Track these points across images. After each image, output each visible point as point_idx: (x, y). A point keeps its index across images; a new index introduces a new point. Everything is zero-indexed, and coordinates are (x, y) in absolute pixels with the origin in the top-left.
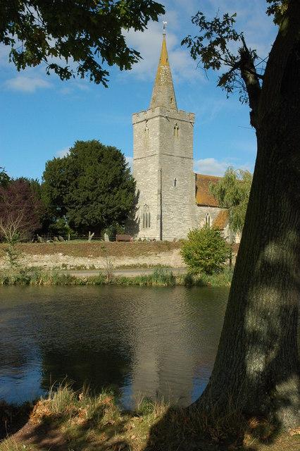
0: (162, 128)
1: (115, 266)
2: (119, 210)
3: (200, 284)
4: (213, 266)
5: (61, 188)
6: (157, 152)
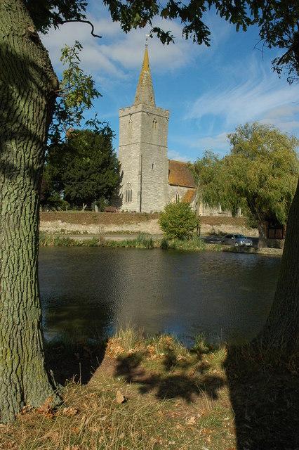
0: (143, 119)
2: (107, 186)
3: (174, 248)
4: (184, 234)
6: (139, 141)
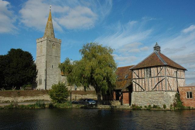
0: (47, 43)
1: (23, 100)
2: (28, 77)
3: (56, 107)
4: (62, 99)
5: (2, 67)
6: (45, 54)
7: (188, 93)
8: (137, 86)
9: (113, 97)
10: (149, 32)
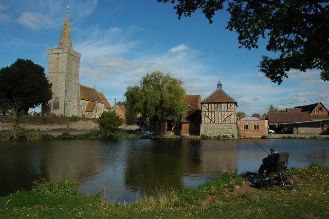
6: (65, 71)
7: (245, 126)
8: (206, 118)
9: (164, 126)
10: (133, 44)
